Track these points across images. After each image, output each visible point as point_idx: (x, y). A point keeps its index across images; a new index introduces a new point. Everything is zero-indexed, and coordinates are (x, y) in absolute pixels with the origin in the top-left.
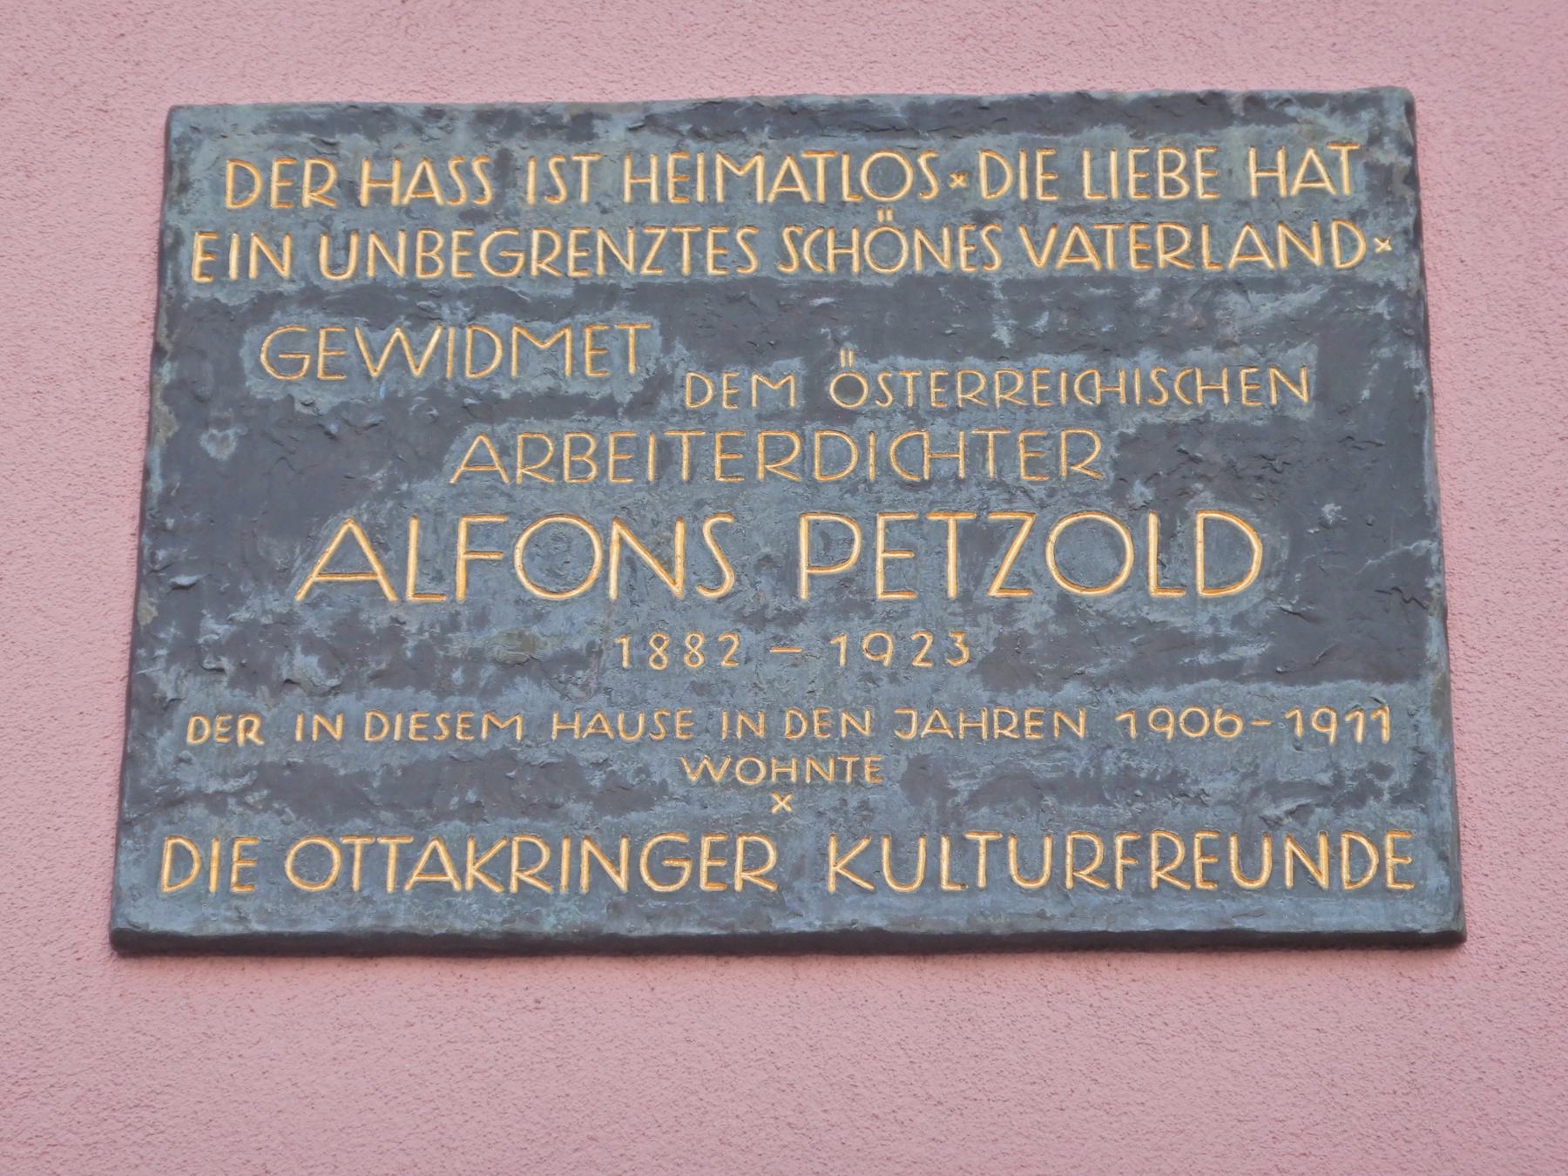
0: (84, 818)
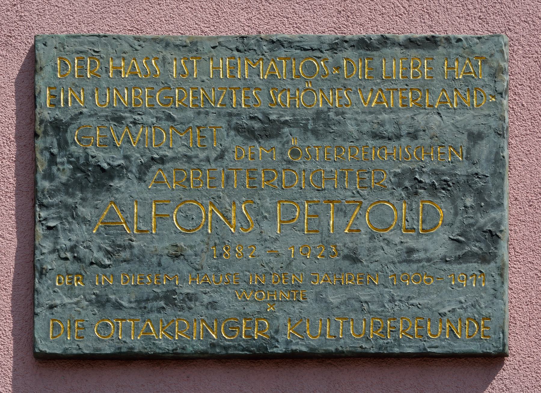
0: (22, 312)
